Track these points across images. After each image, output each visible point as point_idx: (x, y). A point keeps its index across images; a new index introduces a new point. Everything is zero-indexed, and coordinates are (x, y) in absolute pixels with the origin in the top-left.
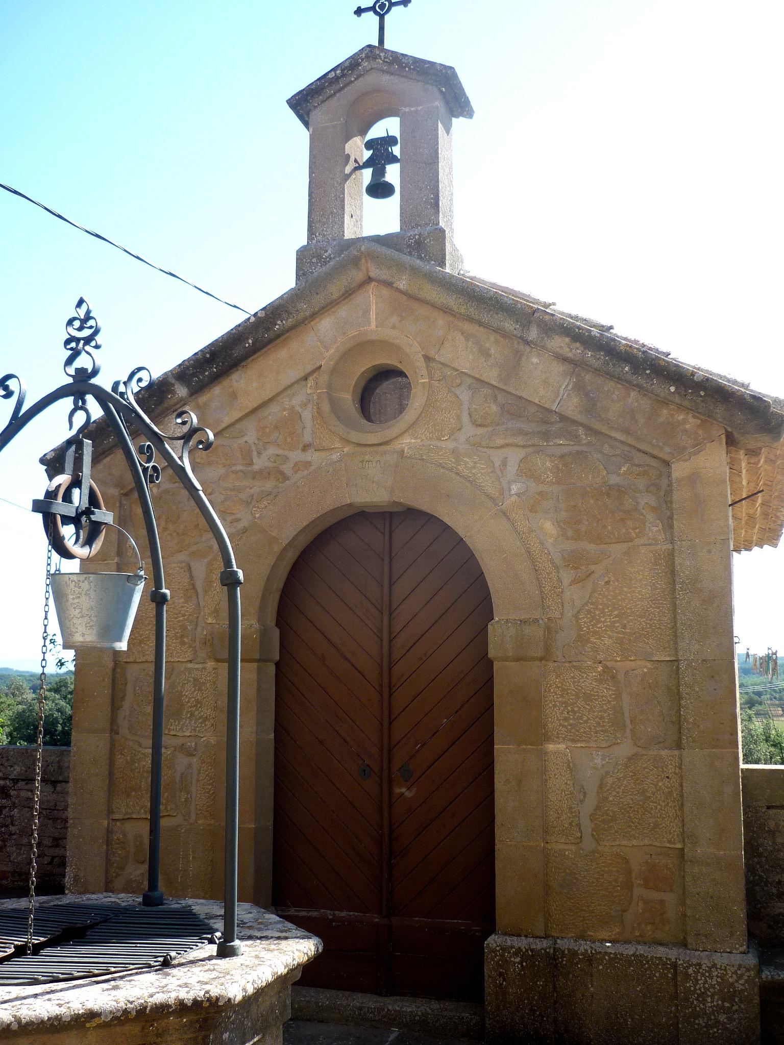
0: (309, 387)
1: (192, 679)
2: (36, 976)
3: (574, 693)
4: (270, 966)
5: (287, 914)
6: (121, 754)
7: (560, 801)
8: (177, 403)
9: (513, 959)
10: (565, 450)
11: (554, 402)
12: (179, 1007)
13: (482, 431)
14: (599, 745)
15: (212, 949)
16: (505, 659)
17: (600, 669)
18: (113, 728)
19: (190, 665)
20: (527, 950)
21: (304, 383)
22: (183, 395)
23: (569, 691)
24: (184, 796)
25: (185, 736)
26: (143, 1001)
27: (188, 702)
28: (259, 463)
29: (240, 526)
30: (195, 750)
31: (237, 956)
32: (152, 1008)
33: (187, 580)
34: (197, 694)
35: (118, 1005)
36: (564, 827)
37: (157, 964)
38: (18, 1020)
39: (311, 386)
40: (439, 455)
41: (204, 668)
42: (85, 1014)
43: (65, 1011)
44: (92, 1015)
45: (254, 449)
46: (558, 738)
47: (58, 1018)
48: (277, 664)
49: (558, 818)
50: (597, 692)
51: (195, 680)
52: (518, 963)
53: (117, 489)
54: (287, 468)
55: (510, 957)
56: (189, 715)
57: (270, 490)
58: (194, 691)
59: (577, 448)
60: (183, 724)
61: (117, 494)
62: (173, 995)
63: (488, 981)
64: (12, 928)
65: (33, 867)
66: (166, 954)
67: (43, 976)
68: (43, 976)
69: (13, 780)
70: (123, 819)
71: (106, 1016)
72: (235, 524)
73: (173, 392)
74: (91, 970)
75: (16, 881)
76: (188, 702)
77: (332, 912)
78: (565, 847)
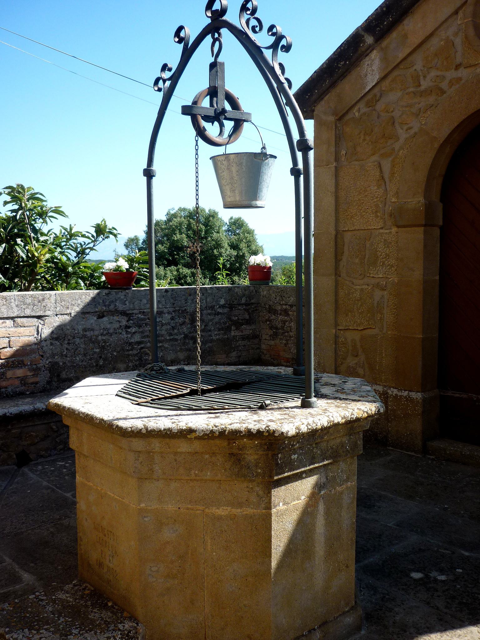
0: (459, 20)
1: (383, 240)
2: (180, 406)
4: (328, 416)
6: (342, 289)
8: (368, 49)
12: (247, 433)
15: (299, 403)
18: (337, 273)
19: (381, 231)
21: (455, 16)
22: (371, 43)
24: (379, 315)
25: (379, 278)
26: (224, 427)
27: (381, 255)
28: (425, 84)
29: (412, 132)
30: (386, 286)
31: (313, 408)
32: (229, 432)
33: (378, 174)
34: (386, 250)
35: (208, 427)
37: (255, 407)
38: (146, 429)
39: (461, 18)
41: (391, 232)
42: (186, 429)
43: (174, 426)
44: (191, 431)
45: (421, 74)
47: (170, 430)
48: (442, 228)
51: (385, 240)
53: (334, 116)
54: (444, 85)
56: (381, 264)
58: (385, 248)
60: (378, 270)
61: (334, 120)
62: (244, 426)
64: (206, 381)
65: (199, 344)
66: (263, 401)
67: (183, 406)
68: (183, 406)
69: (290, 305)
70: (344, 329)
71: (200, 433)
73: (364, 42)
74: (213, 406)
75: (294, 364)
76: (381, 255)
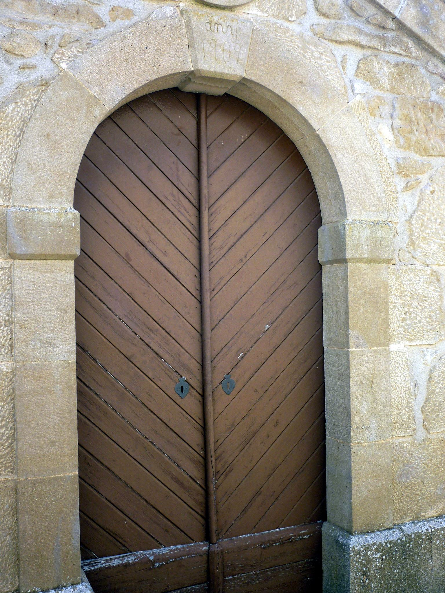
3: (409, 294)
5: (96, 567)
7: (401, 397)
9: (374, 556)
10: (401, 59)
11: (396, 7)
13: (324, 21)
14: (429, 343)
16: (360, 261)
17: (429, 272)
20: (386, 544)
23: (406, 293)
36: (403, 421)
40: (286, 37)
46: (398, 338)
49: (399, 413)
50: (427, 293)
52: (379, 558)
55: (373, 554)
57: (78, 34)
59: (407, 60)
63: (353, 583)
72: (27, 71)
77: (150, 552)
78: (404, 440)
